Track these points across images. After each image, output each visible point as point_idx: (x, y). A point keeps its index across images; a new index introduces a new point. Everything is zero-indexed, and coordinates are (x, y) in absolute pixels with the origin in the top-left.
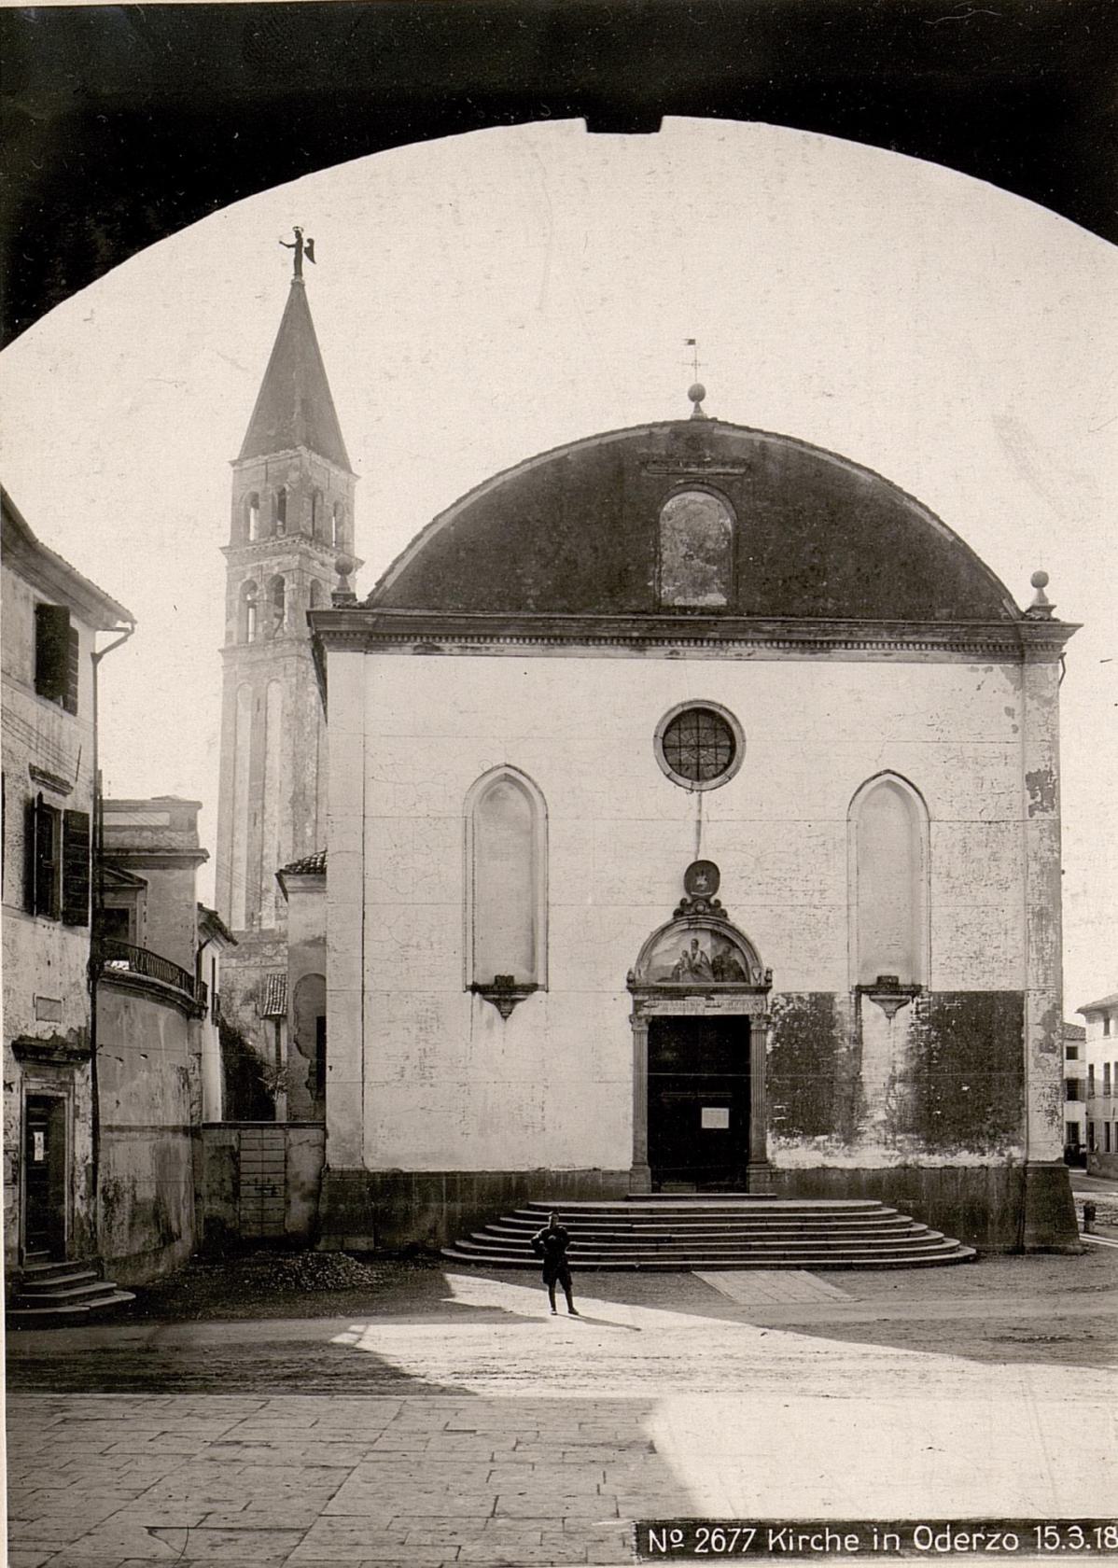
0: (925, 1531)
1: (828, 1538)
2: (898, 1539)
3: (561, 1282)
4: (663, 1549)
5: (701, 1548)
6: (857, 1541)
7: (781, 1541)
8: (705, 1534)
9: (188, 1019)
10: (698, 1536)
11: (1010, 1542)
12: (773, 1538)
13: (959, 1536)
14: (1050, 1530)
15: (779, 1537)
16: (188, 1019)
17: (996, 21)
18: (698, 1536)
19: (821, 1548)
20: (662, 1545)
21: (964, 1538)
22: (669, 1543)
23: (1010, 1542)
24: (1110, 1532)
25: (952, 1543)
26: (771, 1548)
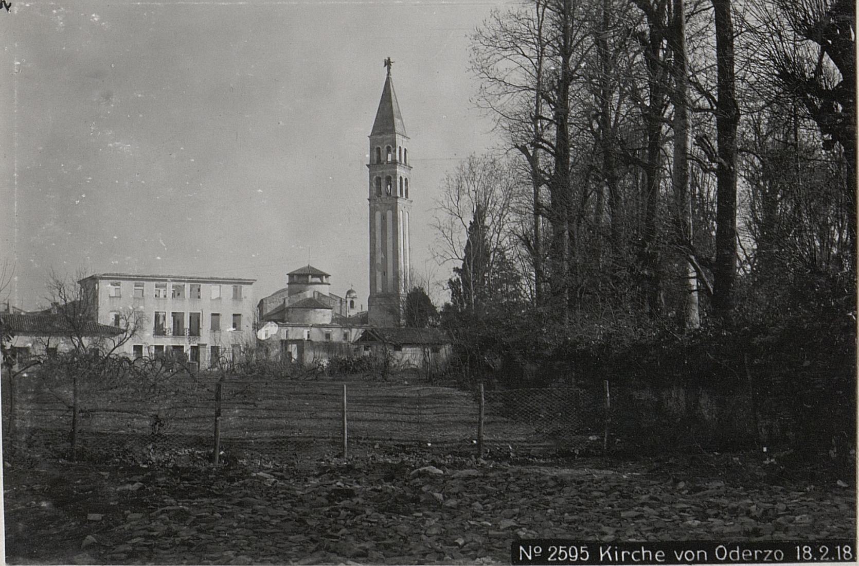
0: (690, 553)
1: (643, 552)
2: (706, 553)
3: (828, 53)
4: (530, 558)
5: (679, 557)
6: (664, 555)
7: (609, 554)
8: (554, 550)
9: (165, 335)
10: (550, 550)
11: (779, 555)
12: (603, 553)
13: (744, 551)
14: (574, 558)
15: (607, 552)
16: (165, 335)
17: (728, 297)
18: (550, 550)
19: (639, 560)
20: (529, 555)
21: (660, 554)
22: (533, 553)
23: (779, 555)
24: (807, 549)
25: (741, 555)
26: (601, 559)
